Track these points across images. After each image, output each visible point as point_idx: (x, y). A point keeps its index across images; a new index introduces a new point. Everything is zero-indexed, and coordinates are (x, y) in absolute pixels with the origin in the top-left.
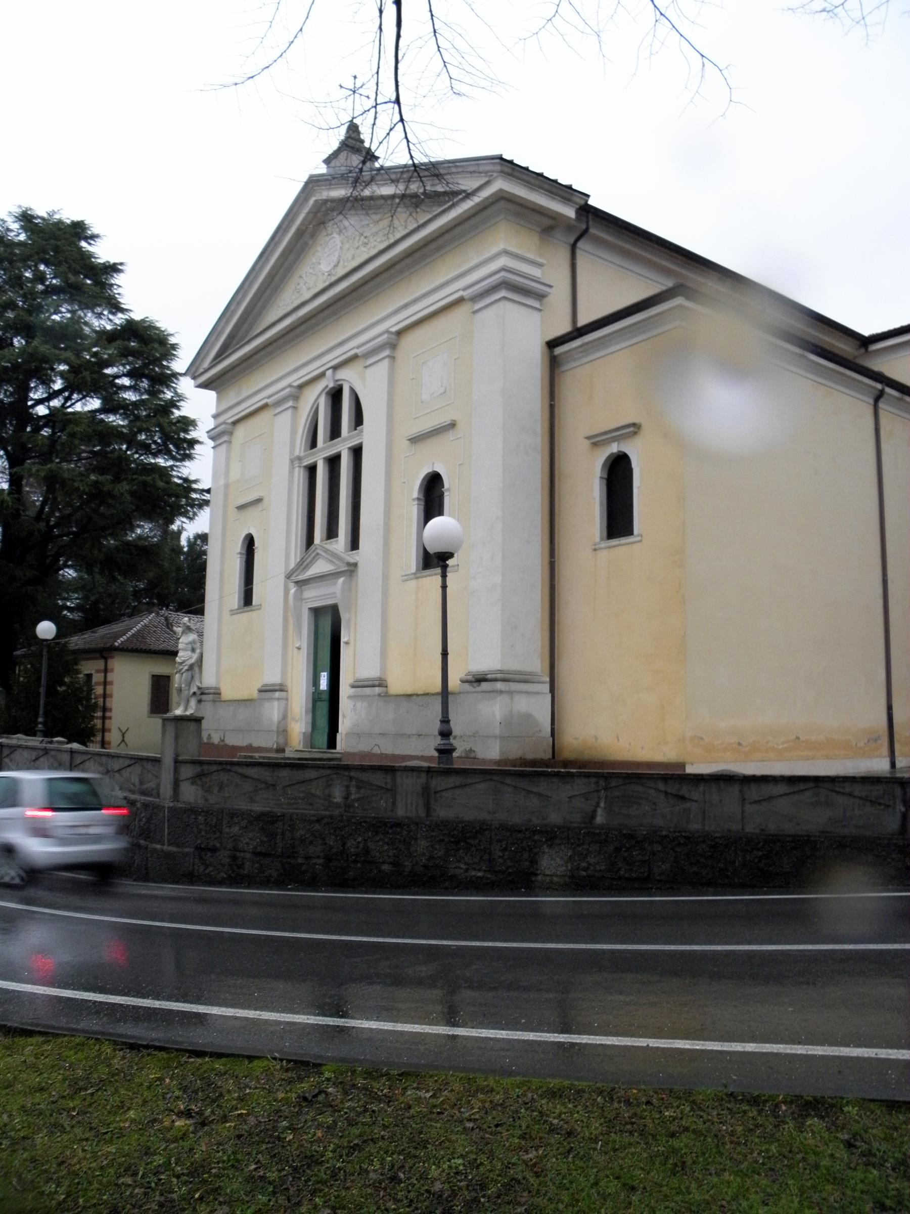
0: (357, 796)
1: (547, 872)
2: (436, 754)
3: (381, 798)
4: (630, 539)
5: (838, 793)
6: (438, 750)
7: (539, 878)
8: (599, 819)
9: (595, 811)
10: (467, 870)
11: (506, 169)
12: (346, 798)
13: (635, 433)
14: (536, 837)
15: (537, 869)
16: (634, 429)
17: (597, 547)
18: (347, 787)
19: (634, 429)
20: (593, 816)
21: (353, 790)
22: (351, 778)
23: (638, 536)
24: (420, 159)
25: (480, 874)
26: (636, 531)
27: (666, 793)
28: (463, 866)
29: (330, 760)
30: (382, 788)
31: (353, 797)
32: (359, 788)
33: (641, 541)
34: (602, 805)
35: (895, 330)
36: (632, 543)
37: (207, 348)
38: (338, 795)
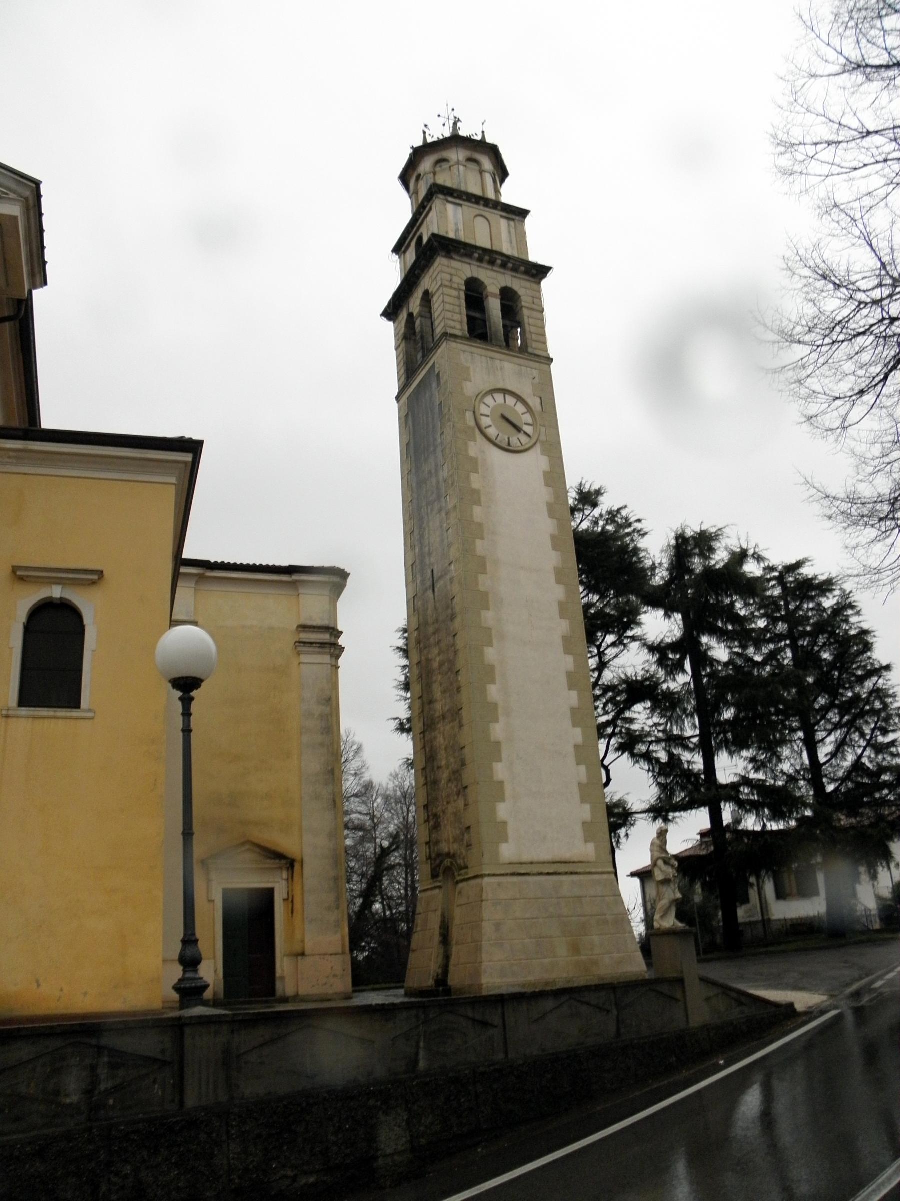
0: (110, 1084)
1: (389, 1151)
2: (176, 996)
3: (155, 1082)
4: (75, 713)
5: (583, 1003)
6: (177, 988)
7: (381, 1162)
8: (422, 1064)
9: (417, 1054)
10: (294, 1179)
11: (31, 202)
12: (89, 1092)
13: (94, 583)
14: (372, 1102)
15: (378, 1150)
16: (94, 578)
17: (11, 712)
18: (93, 1068)
19: (94, 578)
20: (416, 1062)
21: (103, 1072)
22: (100, 1049)
23: (90, 710)
24: (494, 248)
25: (312, 1180)
26: (84, 703)
27: (474, 1020)
28: (290, 1173)
29: (390, 988)
30: (155, 1060)
31: (102, 1087)
32: (113, 1066)
33: (92, 718)
34: (422, 1044)
35: (274, 566)
36: (77, 718)
37: (33, 220)
38: (73, 1086)
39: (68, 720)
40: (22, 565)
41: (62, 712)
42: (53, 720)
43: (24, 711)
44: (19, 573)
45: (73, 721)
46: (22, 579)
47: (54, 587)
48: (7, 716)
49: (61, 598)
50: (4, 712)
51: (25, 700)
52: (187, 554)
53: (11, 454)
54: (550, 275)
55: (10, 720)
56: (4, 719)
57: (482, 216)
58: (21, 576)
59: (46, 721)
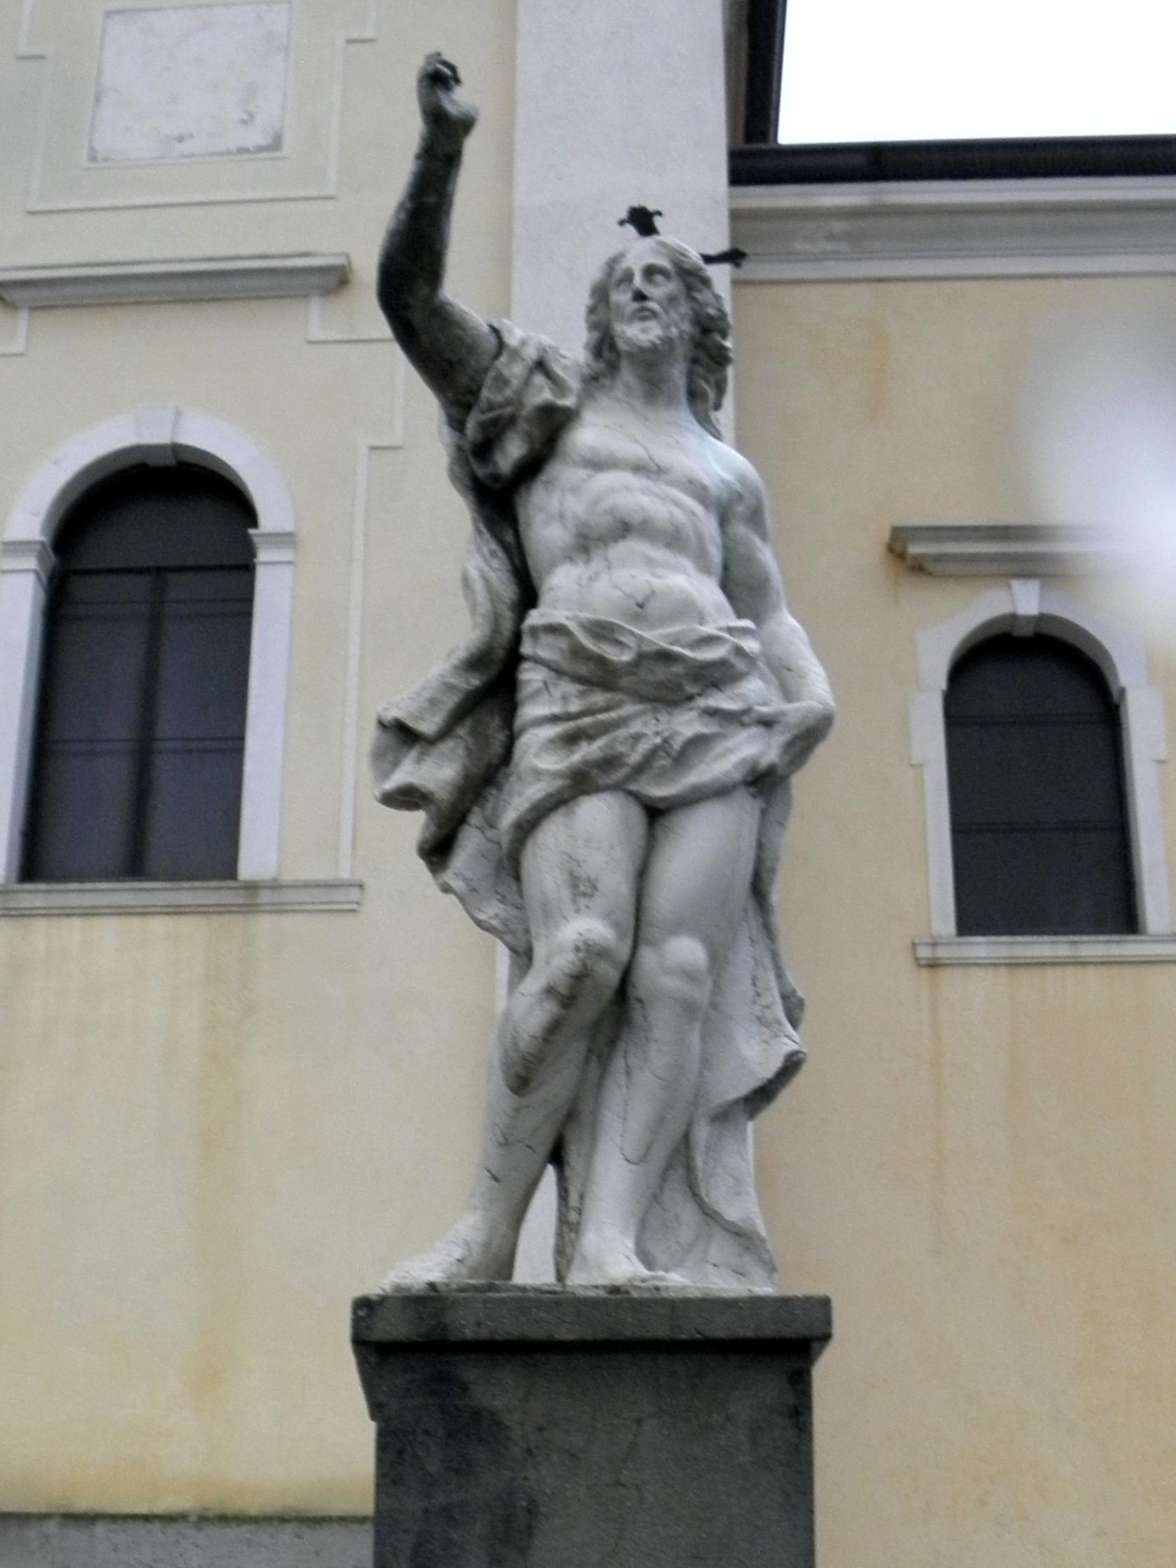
17: (942, 953)
39: (1115, 970)
40: (469, 919)
41: (1095, 947)
42: (1070, 972)
43: (981, 947)
44: (914, 549)
45: (1129, 973)
46: (919, 568)
47: (1017, 585)
48: (934, 965)
49: (1042, 618)
50: (924, 952)
51: (972, 919)
52: (800, 122)
53: (838, 226)
54: (391, 714)
55: (944, 974)
56: (925, 973)
57: (527, 827)
58: (913, 556)
59: (1050, 973)
